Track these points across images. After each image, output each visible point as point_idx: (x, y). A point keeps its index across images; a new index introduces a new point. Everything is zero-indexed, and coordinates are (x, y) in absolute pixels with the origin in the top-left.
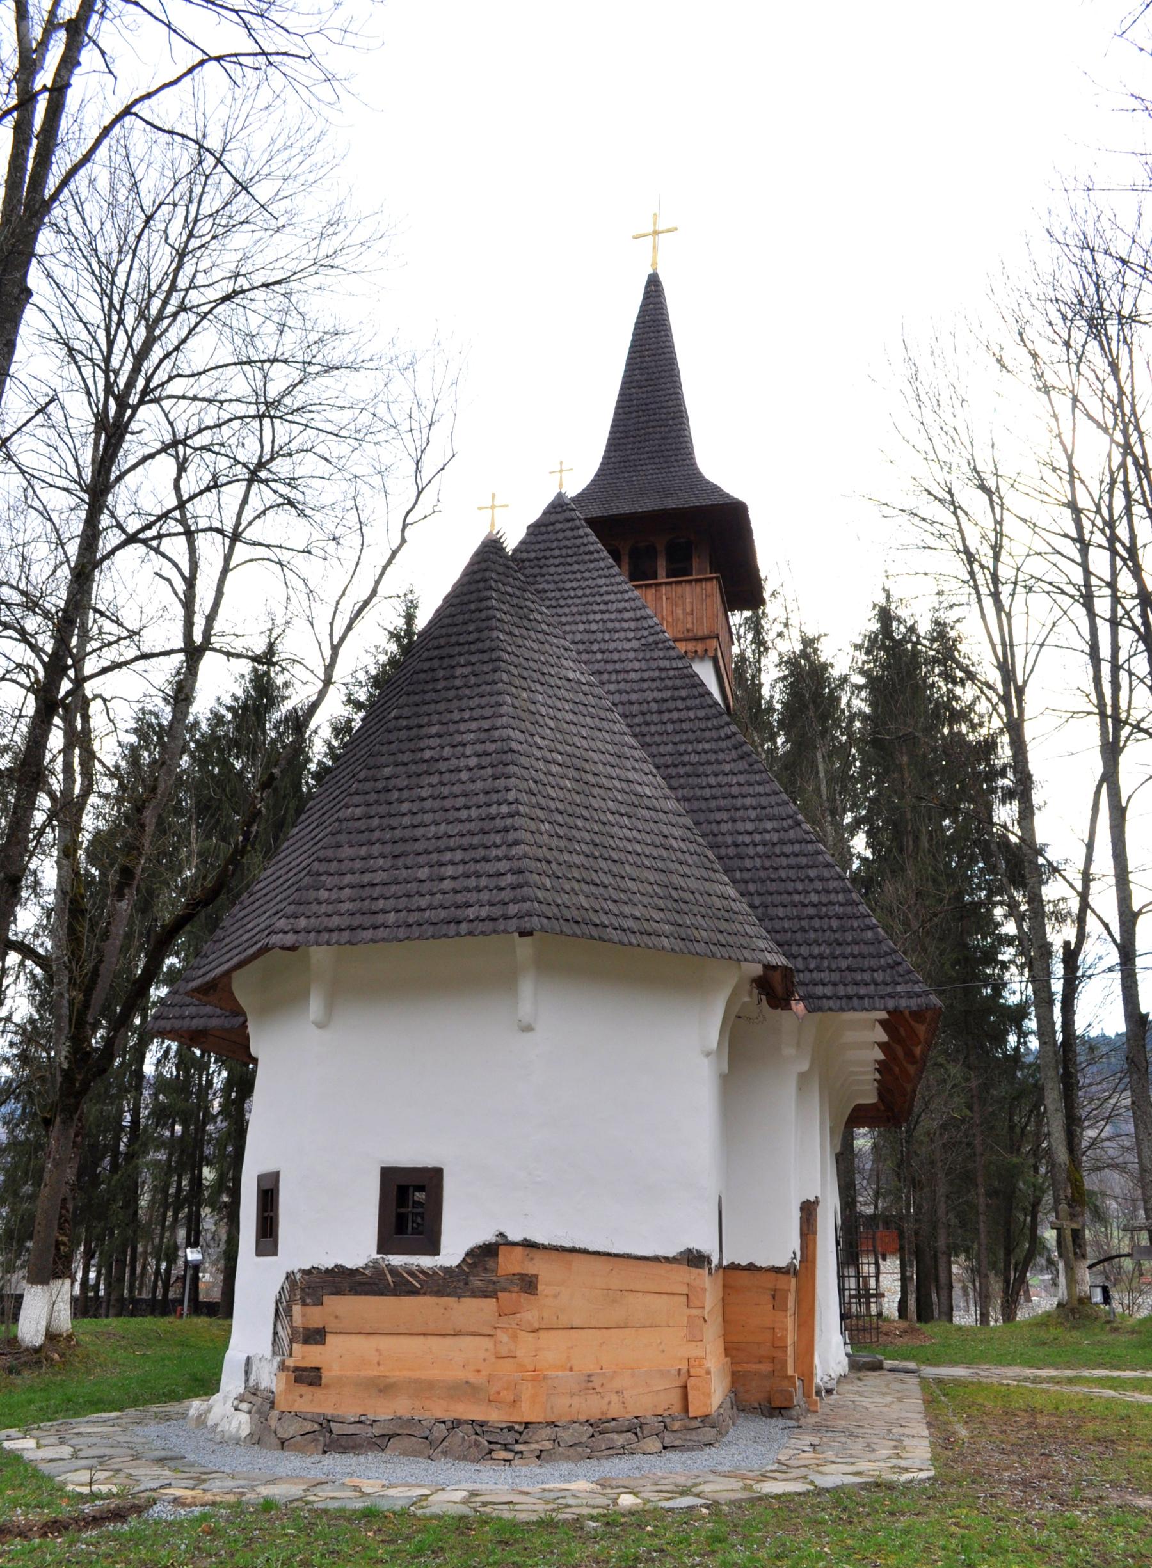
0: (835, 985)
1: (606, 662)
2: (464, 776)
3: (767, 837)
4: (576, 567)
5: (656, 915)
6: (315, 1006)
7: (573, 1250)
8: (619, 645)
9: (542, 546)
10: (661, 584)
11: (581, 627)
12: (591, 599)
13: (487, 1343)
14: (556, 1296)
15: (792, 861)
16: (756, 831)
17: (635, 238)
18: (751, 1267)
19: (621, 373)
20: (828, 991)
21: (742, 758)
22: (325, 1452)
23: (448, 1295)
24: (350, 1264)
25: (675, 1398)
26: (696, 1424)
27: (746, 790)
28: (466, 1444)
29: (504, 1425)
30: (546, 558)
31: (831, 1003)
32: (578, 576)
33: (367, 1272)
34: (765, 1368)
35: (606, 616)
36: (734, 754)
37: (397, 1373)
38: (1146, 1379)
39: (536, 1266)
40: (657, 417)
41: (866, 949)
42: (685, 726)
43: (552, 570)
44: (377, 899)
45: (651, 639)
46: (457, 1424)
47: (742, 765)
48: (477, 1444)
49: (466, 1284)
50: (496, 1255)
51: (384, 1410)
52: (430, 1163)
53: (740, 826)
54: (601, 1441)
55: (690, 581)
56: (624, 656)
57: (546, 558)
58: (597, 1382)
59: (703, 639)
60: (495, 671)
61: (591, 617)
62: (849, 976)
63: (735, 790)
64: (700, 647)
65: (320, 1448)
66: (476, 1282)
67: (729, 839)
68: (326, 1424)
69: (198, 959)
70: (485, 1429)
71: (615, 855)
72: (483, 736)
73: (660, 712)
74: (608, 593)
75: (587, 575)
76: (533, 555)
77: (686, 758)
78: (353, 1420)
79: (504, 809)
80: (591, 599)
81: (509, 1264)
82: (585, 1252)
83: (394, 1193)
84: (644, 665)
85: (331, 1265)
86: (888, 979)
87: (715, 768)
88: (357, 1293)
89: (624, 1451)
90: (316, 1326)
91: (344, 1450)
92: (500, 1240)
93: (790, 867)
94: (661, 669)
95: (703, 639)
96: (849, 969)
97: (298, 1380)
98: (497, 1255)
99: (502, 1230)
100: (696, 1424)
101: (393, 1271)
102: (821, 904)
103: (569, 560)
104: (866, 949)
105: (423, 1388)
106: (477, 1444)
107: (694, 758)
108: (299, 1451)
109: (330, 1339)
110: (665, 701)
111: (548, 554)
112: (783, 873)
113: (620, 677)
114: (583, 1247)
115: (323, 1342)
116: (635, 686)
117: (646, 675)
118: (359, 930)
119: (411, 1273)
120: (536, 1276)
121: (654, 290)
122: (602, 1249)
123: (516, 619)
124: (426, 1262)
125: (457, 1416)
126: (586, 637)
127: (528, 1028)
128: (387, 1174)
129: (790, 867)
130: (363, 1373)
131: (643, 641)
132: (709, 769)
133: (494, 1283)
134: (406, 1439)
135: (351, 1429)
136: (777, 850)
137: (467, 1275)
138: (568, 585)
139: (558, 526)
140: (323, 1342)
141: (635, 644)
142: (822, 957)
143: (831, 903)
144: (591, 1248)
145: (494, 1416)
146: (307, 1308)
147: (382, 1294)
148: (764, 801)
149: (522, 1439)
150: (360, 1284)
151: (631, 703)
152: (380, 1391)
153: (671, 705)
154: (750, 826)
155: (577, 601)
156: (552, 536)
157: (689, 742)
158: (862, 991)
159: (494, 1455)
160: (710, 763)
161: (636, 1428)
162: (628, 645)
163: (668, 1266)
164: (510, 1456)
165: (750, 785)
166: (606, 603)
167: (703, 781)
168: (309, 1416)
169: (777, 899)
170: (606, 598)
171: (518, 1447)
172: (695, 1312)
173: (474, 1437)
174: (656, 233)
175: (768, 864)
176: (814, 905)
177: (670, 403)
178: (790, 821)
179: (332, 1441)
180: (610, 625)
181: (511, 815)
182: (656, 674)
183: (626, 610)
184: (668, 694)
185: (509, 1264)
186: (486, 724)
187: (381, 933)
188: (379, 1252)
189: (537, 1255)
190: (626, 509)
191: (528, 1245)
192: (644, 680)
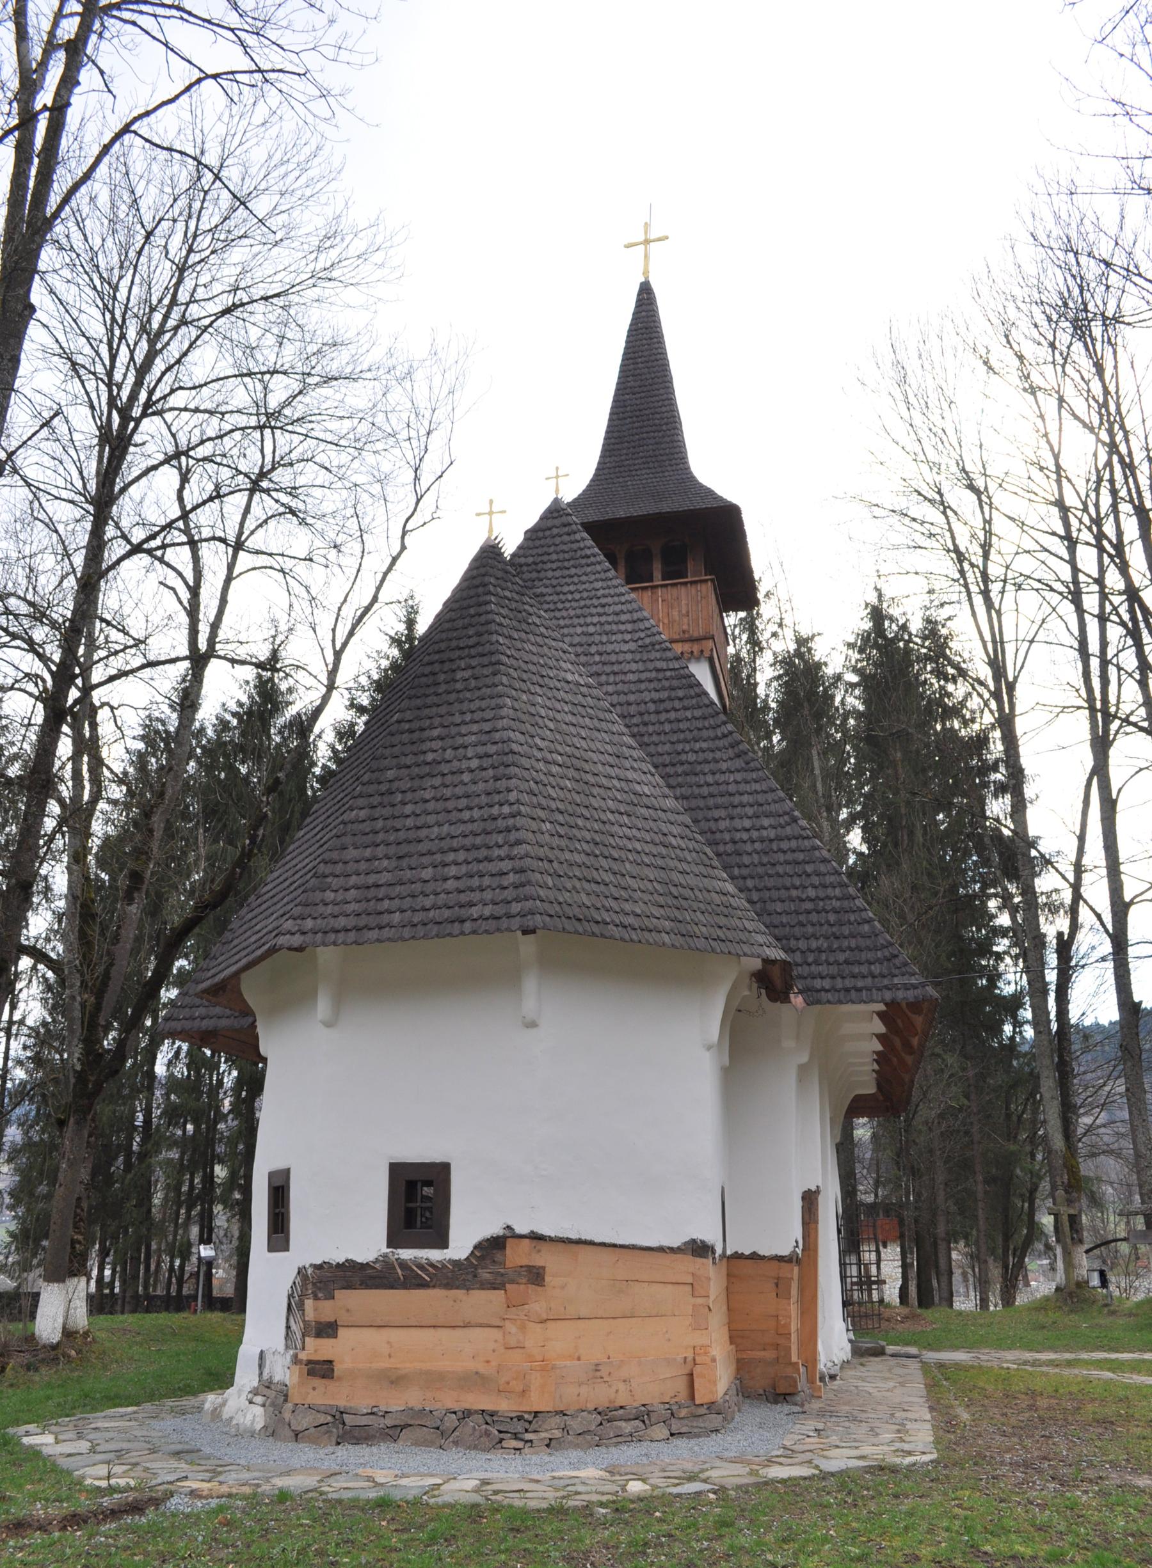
1: (604, 664)
2: (466, 777)
3: (765, 833)
4: (573, 571)
6: (323, 1006)
7: (579, 1242)
11: (579, 630)
12: (588, 602)
13: (496, 1334)
14: (563, 1287)
15: (789, 856)
16: (753, 827)
18: (754, 1256)
20: (827, 983)
21: (738, 756)
22: (338, 1444)
23: (457, 1288)
24: (360, 1259)
25: (681, 1386)
28: (477, 1434)
29: (514, 1415)
30: (544, 563)
31: (829, 996)
32: (576, 580)
33: (377, 1266)
34: (770, 1355)
35: (603, 619)
39: (544, 1258)
40: (651, 422)
41: (863, 943)
45: (647, 641)
46: (467, 1414)
48: (487, 1434)
49: (475, 1276)
50: (504, 1247)
51: (396, 1402)
53: (738, 824)
54: (609, 1429)
56: (621, 657)
59: (698, 640)
60: (494, 674)
62: (847, 969)
63: (732, 788)
64: (696, 648)
65: (334, 1440)
66: (484, 1274)
68: (339, 1415)
70: (495, 1418)
74: (605, 596)
77: (684, 757)
78: (365, 1411)
79: (506, 809)
80: (588, 602)
81: (517, 1256)
82: (591, 1243)
83: (402, 1188)
84: (641, 666)
85: (341, 1260)
86: (885, 971)
87: (712, 766)
88: (368, 1287)
89: (632, 1438)
91: (357, 1441)
92: (508, 1233)
93: (787, 863)
94: (658, 670)
95: (698, 640)
97: (311, 1373)
98: (504, 1248)
99: (510, 1223)
100: (703, 1411)
101: (403, 1264)
103: (566, 564)
104: (863, 943)
105: (434, 1379)
106: (487, 1434)
107: (692, 757)
109: (341, 1332)
110: (662, 701)
111: (545, 558)
112: (780, 869)
113: (618, 678)
114: (588, 1238)
117: (644, 676)
118: (365, 931)
119: (421, 1267)
120: (544, 1268)
121: (646, 298)
122: (607, 1241)
123: (515, 623)
125: (468, 1406)
126: (584, 639)
127: (532, 1025)
128: (397, 1170)
129: (787, 863)
130: (375, 1366)
132: (706, 768)
133: (502, 1275)
134: (418, 1430)
135: (364, 1421)
138: (566, 589)
139: (555, 531)
141: (632, 646)
142: (820, 950)
143: (829, 898)
144: (597, 1240)
145: (504, 1406)
147: (392, 1288)
148: (761, 798)
150: (371, 1277)
151: (629, 704)
152: (392, 1382)
154: (747, 823)
155: (574, 604)
157: (687, 741)
159: (504, 1444)
162: (625, 647)
164: (520, 1444)
165: (747, 782)
166: (603, 606)
167: (701, 779)
168: (322, 1408)
169: (775, 894)
170: (603, 601)
171: (528, 1436)
173: (484, 1426)
175: (765, 860)
176: (812, 900)
177: (664, 409)
180: (607, 628)
182: (654, 674)
183: (622, 612)
185: (517, 1256)
187: (386, 932)
188: (388, 1247)
189: (544, 1247)
190: (621, 513)
191: (535, 1237)
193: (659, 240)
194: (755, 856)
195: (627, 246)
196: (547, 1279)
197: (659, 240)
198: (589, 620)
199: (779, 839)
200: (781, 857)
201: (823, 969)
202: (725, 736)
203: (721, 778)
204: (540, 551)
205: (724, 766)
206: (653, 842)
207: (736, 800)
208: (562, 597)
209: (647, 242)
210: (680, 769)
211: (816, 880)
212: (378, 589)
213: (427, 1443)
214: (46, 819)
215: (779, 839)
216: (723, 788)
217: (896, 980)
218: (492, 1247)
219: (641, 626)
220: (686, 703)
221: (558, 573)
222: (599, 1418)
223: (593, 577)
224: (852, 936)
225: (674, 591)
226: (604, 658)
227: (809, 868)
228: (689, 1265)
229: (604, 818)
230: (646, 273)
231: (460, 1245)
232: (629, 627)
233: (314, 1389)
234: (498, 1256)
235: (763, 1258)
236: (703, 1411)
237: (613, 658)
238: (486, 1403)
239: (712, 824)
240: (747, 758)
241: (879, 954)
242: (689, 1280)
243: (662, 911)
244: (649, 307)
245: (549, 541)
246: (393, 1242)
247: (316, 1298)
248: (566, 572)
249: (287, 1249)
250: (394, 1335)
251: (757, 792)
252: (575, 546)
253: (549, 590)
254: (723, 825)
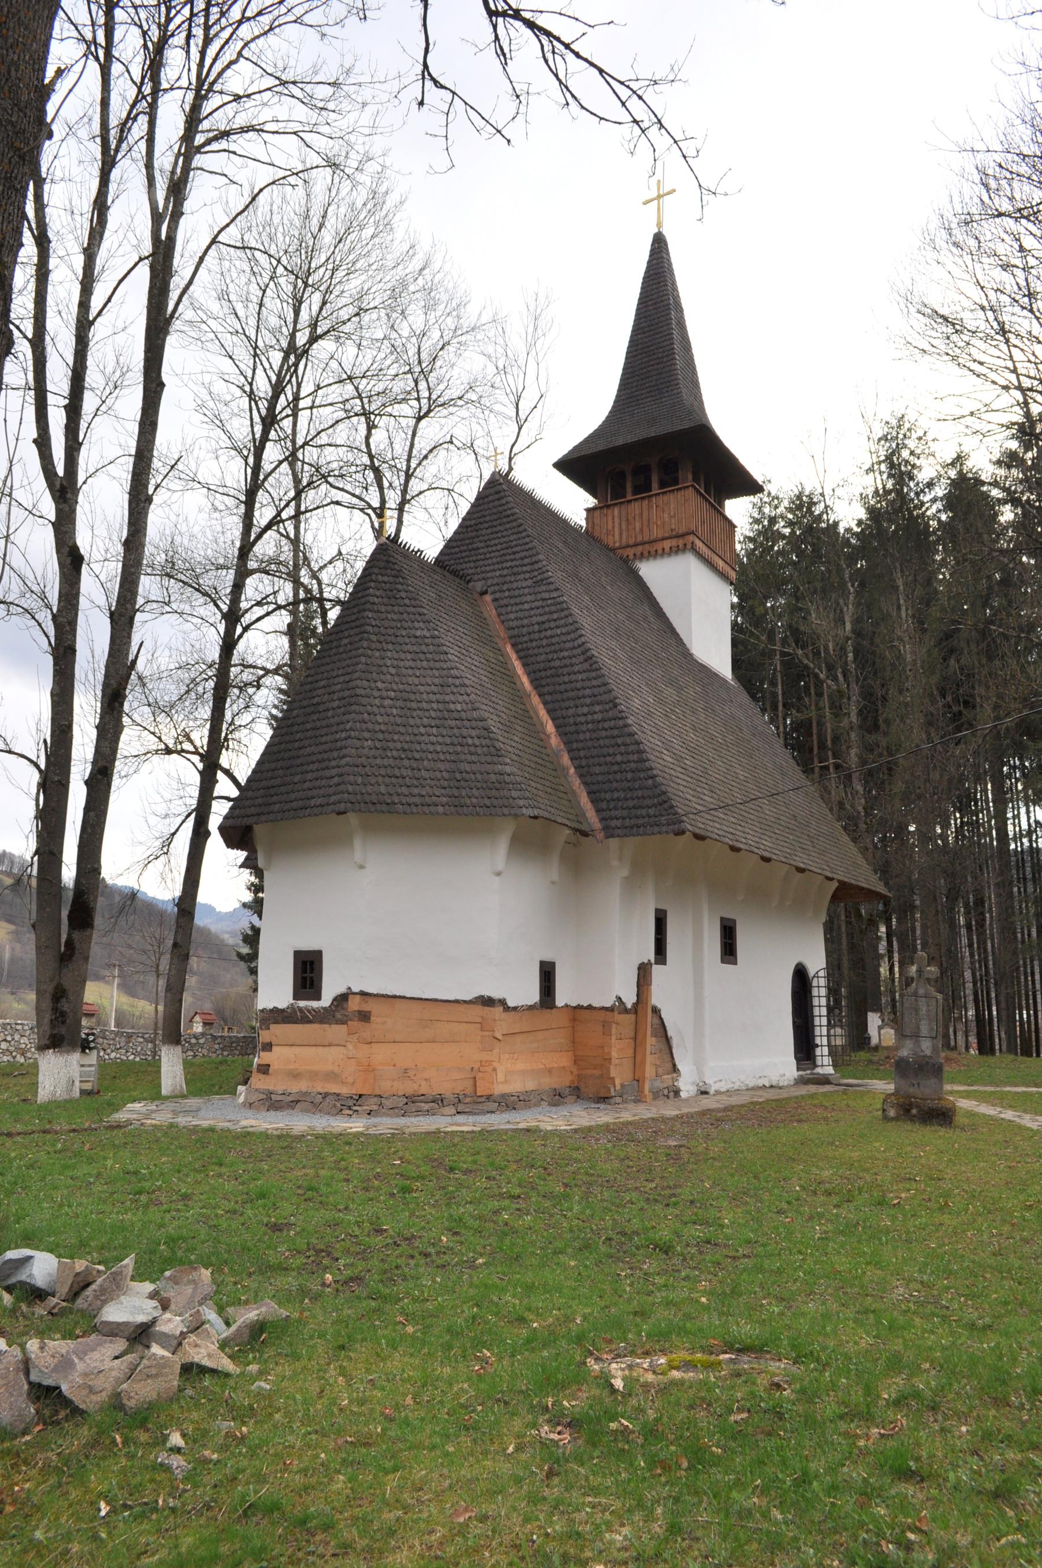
0: (624, 818)
1: (511, 597)
2: (330, 714)
3: (596, 716)
4: (499, 528)
5: (437, 792)
7: (395, 997)
8: (519, 584)
10: (630, 501)
11: (498, 573)
12: (505, 551)
14: (384, 1023)
15: (609, 733)
16: (589, 713)
18: (590, 1007)
19: (632, 323)
20: (619, 823)
21: (586, 661)
24: (280, 1007)
25: (469, 1084)
26: (480, 1100)
27: (588, 684)
31: (619, 831)
32: (499, 535)
34: (597, 1072)
35: (514, 563)
36: (582, 658)
40: (655, 357)
41: (646, 793)
42: (554, 640)
43: (484, 532)
45: (539, 578)
46: (326, 1095)
47: (586, 666)
50: (347, 1000)
51: (295, 1087)
53: (580, 711)
54: (413, 1107)
55: (680, 489)
56: (521, 592)
58: (411, 1073)
59: (683, 535)
60: (360, 640)
61: (505, 565)
62: (634, 812)
63: (579, 685)
64: (681, 543)
67: (572, 720)
71: (417, 756)
72: (345, 686)
73: (540, 632)
74: (516, 546)
75: (505, 533)
76: (473, 522)
77: (552, 664)
79: (344, 735)
80: (505, 551)
81: (354, 1004)
82: (404, 997)
83: (300, 965)
84: (533, 598)
85: (271, 1007)
86: (657, 813)
87: (569, 669)
88: (285, 1023)
93: (607, 737)
94: (543, 600)
95: (683, 535)
96: (634, 807)
100: (482, 1099)
101: (301, 1010)
102: (623, 762)
103: (495, 523)
104: (646, 793)
105: (313, 1075)
106: (335, 1106)
107: (557, 663)
109: (274, 1048)
110: (543, 623)
112: (602, 742)
113: (518, 608)
114: (402, 994)
115: (271, 1050)
116: (526, 614)
117: (534, 605)
119: (309, 1011)
120: (370, 1012)
121: (659, 244)
122: (430, 997)
123: (385, 600)
124: (314, 1004)
126: (501, 580)
127: (362, 867)
128: (297, 954)
129: (607, 737)
131: (534, 580)
132: (565, 670)
135: (280, 1098)
136: (600, 726)
138: (493, 543)
139: (491, 498)
140: (271, 1050)
141: (529, 582)
142: (618, 799)
143: (629, 761)
144: (408, 995)
145: (344, 1091)
148: (596, 691)
149: (359, 1102)
151: (523, 627)
153: (547, 625)
154: (585, 710)
155: (497, 554)
156: (486, 507)
157: (555, 652)
158: (640, 821)
160: (566, 666)
161: (439, 1101)
162: (524, 584)
163: (466, 1005)
164: (351, 1112)
165: (589, 680)
166: (514, 553)
167: (561, 679)
169: (596, 760)
170: (515, 549)
171: (355, 1108)
172: (486, 1033)
174: (659, 197)
175: (594, 735)
176: (618, 764)
177: (665, 343)
178: (611, 705)
180: (515, 570)
181: (346, 739)
182: (540, 603)
183: (526, 557)
184: (546, 617)
185: (354, 1004)
186: (347, 678)
187: (271, 817)
191: (363, 994)
192: (532, 609)
193: (669, 193)
194: (588, 734)
195: (645, 203)
196: (372, 1018)
197: (669, 193)
198: (505, 565)
199: (604, 720)
200: (603, 734)
201: (618, 813)
202: (579, 646)
203: (573, 677)
204: (479, 515)
205: (576, 668)
206: (452, 744)
207: (580, 693)
208: (490, 549)
209: (659, 197)
210: (549, 672)
211: (623, 749)
213: (307, 1111)
214: (953, 477)
215: (604, 720)
216: (573, 685)
218: (342, 999)
219: (536, 566)
220: (558, 623)
221: (489, 531)
222: (405, 1100)
223: (510, 532)
224: (640, 788)
225: (666, 498)
226: (512, 593)
227: (619, 741)
228: (480, 1010)
229: (416, 732)
230: (659, 224)
231: (326, 1000)
232: (528, 568)
235: (595, 1008)
236: (482, 1099)
237: (517, 592)
239: (564, 712)
240: (591, 662)
241: (656, 800)
242: (479, 1020)
243: (443, 791)
244: (659, 255)
245: (486, 507)
246: (297, 996)
248: (495, 529)
250: (297, 1050)
251: (594, 687)
252: (500, 509)
253: (482, 545)
254: (571, 712)
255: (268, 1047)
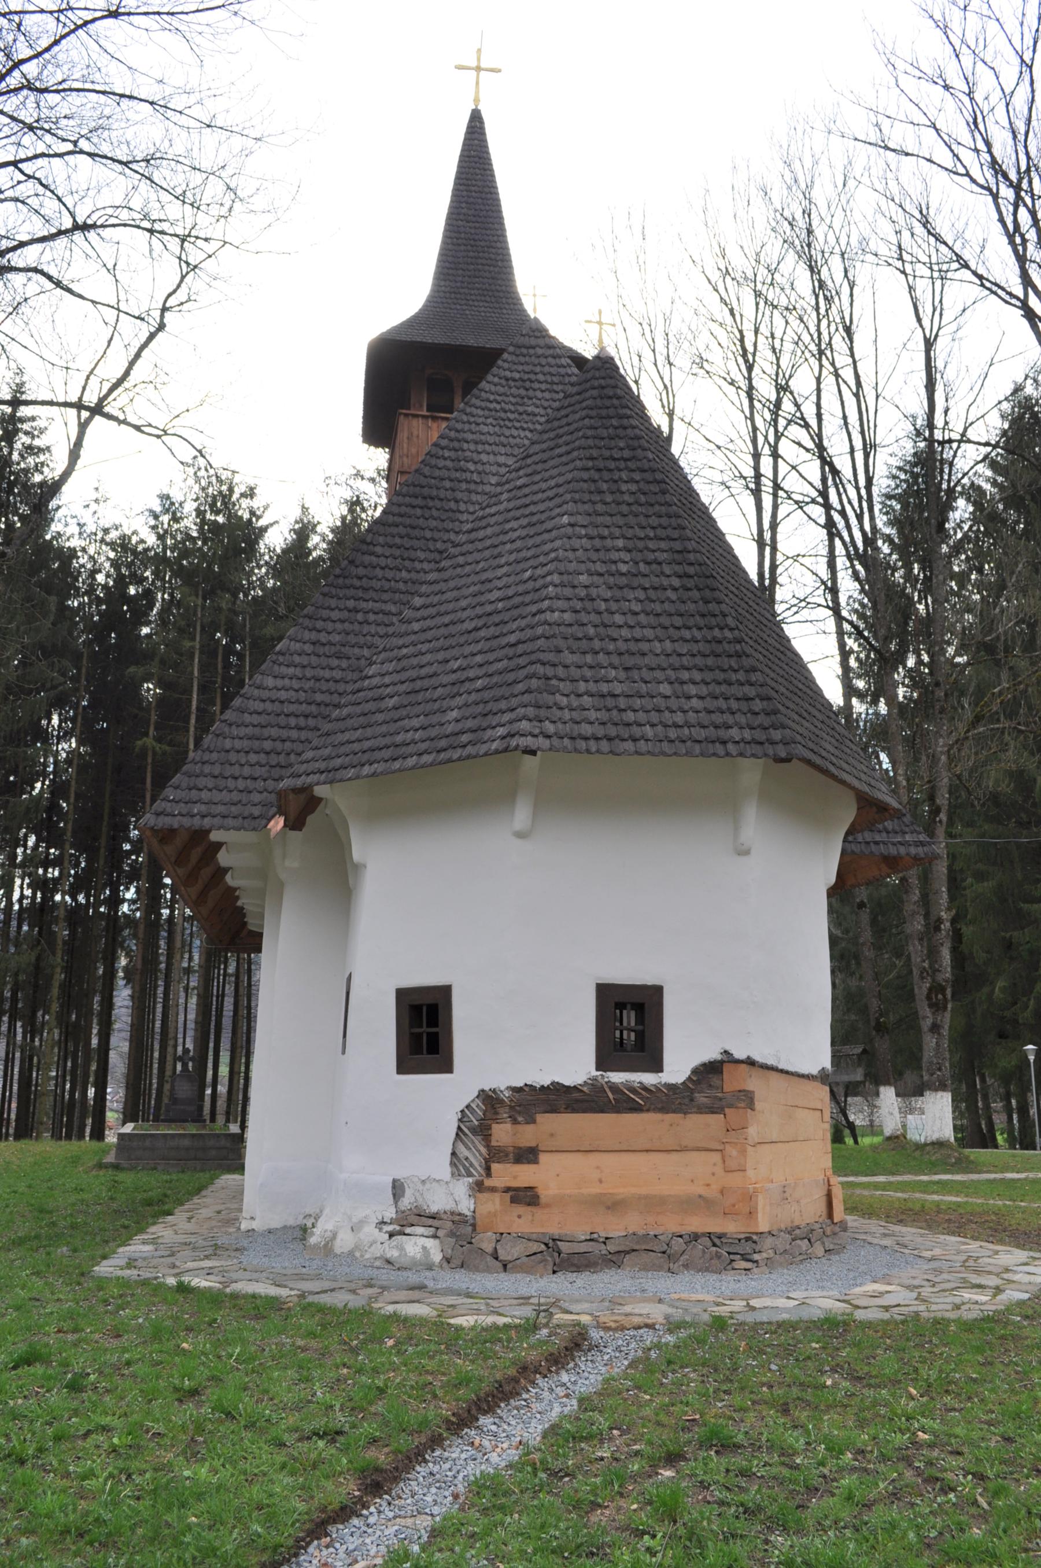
6: (522, 815)
9: (527, 368)
13: (716, 1157)
17: (499, 71)
22: (554, 1272)
23: (674, 1112)
28: (707, 1256)
29: (742, 1236)
30: (531, 381)
33: (585, 1089)
37: (621, 1190)
38: (1035, 1181)
39: (754, 1083)
44: (624, 710)
46: (695, 1237)
48: (718, 1256)
49: (692, 1100)
52: (649, 980)
57: (531, 381)
65: (550, 1268)
66: (701, 1098)
68: (552, 1244)
69: (199, 752)
70: (724, 1240)
78: (583, 1238)
85: (546, 1082)
86: (897, 828)
88: (574, 1111)
90: (528, 1145)
91: (578, 1268)
92: (725, 1058)
97: (514, 1200)
98: (722, 1072)
99: (727, 1048)
101: (614, 1088)
103: (555, 387)
105: (654, 1204)
106: (718, 1256)
108: (527, 1272)
109: (543, 1158)
111: (533, 377)
115: (535, 1161)
118: (617, 741)
119: (633, 1090)
124: (649, 1079)
125: (693, 1229)
130: (585, 1191)
133: (721, 1099)
134: (644, 1254)
137: (692, 1091)
140: (535, 1161)
145: (732, 1227)
146: (519, 1127)
147: (602, 1112)
150: (577, 1101)
152: (608, 1208)
159: (736, 1265)
164: (749, 1265)
168: (534, 1236)
173: (714, 1249)
179: (563, 1261)
185: (732, 1081)
187: (642, 745)
188: (597, 1069)
189: (755, 1072)
190: (471, 342)
191: (750, 1062)
212: (132, 364)
217: (908, 837)
230: (477, 100)
233: (519, 1217)
234: (715, 1080)
238: (715, 1226)
246: (602, 1064)
247: (515, 1122)
249: (450, 1070)
255: (528, 1155)
